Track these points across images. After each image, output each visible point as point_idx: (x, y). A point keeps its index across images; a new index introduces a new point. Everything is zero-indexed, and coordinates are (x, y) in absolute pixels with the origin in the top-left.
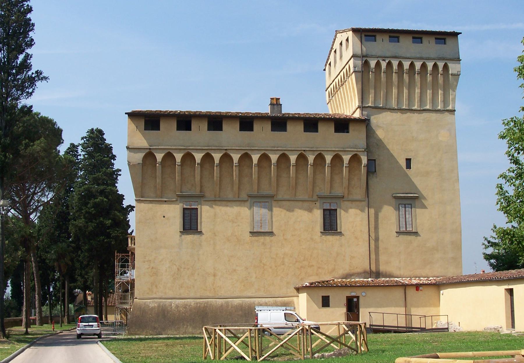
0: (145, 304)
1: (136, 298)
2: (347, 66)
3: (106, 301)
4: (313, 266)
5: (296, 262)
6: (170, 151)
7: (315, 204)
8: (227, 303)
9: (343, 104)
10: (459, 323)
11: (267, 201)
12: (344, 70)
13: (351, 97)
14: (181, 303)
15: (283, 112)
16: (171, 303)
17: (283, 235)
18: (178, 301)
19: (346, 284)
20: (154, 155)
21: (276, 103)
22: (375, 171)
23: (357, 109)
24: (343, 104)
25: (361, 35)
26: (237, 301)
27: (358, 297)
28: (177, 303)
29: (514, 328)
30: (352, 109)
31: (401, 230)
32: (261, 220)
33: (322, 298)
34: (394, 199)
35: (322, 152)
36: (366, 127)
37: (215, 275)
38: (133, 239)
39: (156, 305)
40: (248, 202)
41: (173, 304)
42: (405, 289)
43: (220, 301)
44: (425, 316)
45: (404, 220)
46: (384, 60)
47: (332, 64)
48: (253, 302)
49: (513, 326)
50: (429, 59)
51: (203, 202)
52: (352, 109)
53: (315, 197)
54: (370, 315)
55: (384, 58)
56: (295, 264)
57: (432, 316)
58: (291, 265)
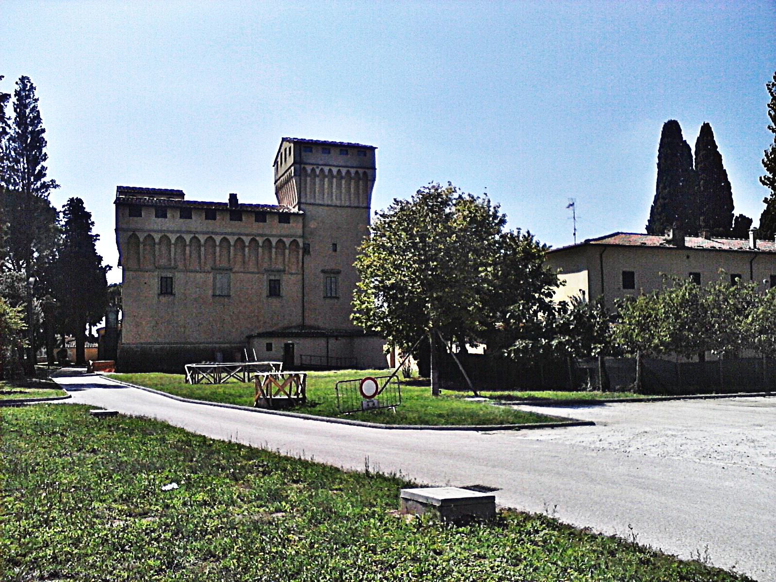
20: (184, 238)
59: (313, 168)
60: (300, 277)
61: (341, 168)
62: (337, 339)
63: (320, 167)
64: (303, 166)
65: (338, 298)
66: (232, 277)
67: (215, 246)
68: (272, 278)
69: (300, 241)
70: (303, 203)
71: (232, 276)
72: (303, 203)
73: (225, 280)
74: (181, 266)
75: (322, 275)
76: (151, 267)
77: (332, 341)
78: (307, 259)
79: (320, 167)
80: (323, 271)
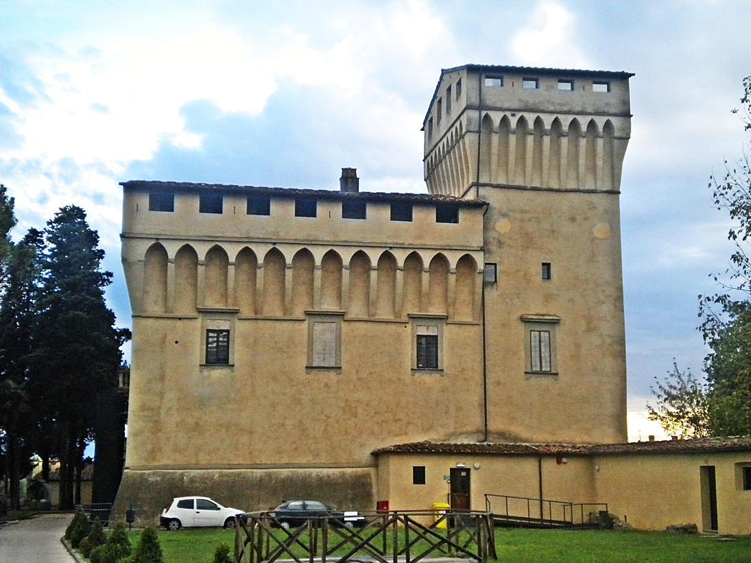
0: (142, 477)
1: (127, 468)
2: (458, 124)
3: (79, 473)
4: (400, 420)
5: (376, 413)
6: (250, 247)
7: (406, 327)
8: (269, 475)
9: (449, 181)
10: (626, 516)
11: (332, 321)
12: (453, 130)
13: (462, 170)
14: (198, 476)
15: (361, 190)
16: (182, 475)
17: (357, 372)
18: (194, 473)
19: (450, 449)
20: (163, 247)
21: (349, 177)
22: (496, 281)
23: (470, 188)
24: (449, 181)
25: (480, 76)
26: (285, 472)
27: (468, 471)
28: (192, 475)
29: (717, 529)
30: (468, 183)
31: (534, 369)
32: (324, 350)
33: (316, 212)
34: (523, 324)
35: (417, 251)
36: (484, 215)
37: (251, 433)
38: (126, 376)
39: (158, 479)
40: (305, 322)
41: (185, 478)
42: (540, 462)
43: (259, 472)
44: (571, 505)
45: (538, 354)
46: (513, 115)
47: (435, 121)
48: (309, 475)
49: (714, 525)
50: (582, 113)
51: (237, 320)
52: (468, 183)
53: (405, 319)
54: (487, 499)
55: (514, 111)
56: (374, 417)
57: (582, 504)
58: (367, 418)
59: (505, 116)
60: (479, 329)
61: (559, 116)
62: (559, 462)
63: (519, 115)
64: (484, 113)
65: (556, 374)
66: (343, 331)
67: (312, 268)
68: (423, 331)
69: (479, 259)
70: (485, 185)
71: (344, 326)
72: (485, 185)
73: (330, 337)
74: (246, 311)
75: (521, 327)
76: (188, 311)
77: (549, 466)
78: (491, 294)
79: (519, 115)
80: (524, 320)
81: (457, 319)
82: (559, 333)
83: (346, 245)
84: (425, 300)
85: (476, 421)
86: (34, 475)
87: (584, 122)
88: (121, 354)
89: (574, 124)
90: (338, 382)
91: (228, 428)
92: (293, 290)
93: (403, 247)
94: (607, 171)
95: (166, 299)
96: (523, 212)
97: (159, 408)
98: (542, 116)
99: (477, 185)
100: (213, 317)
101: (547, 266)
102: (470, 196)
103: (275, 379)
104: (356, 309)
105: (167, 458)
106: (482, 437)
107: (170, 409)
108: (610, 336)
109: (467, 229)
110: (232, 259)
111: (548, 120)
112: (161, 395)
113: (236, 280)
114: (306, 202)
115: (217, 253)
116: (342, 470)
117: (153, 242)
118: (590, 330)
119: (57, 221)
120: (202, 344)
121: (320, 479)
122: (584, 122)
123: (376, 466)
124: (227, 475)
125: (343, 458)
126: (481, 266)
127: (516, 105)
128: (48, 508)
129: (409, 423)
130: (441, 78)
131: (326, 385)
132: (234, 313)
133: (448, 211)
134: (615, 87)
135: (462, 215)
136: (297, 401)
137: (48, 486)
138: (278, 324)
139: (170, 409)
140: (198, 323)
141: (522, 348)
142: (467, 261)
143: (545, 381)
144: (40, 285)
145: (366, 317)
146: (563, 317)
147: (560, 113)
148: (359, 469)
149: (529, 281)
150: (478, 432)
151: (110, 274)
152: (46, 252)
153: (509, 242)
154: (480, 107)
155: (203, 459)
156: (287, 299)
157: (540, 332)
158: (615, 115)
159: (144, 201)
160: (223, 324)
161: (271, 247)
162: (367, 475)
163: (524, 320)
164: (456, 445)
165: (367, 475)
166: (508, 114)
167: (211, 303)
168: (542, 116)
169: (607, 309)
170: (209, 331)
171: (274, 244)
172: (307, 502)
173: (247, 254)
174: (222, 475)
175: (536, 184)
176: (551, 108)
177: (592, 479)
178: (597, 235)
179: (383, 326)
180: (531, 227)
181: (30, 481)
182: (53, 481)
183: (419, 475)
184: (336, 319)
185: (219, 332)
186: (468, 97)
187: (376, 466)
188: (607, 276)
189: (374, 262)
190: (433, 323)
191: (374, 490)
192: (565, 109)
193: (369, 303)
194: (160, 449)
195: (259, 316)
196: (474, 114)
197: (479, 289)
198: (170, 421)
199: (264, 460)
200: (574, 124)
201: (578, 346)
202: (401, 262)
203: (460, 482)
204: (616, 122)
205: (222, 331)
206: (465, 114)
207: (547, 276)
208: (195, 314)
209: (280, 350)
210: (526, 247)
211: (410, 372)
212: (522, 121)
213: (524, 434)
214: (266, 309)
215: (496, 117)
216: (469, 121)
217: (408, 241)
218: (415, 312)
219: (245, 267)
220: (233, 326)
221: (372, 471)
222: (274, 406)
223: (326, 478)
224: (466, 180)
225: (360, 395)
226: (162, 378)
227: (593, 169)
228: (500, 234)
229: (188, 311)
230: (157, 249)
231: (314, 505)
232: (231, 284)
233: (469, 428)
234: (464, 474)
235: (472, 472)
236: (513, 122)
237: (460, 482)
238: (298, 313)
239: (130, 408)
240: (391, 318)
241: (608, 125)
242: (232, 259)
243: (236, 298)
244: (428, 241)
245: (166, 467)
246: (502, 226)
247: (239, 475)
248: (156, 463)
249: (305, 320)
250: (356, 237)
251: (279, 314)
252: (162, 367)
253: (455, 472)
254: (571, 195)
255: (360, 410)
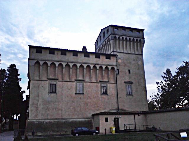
8: (67, 121)
16: (44, 122)
21: (84, 48)
26: (71, 120)
43: (64, 120)
50: (135, 37)
55: (121, 36)
57: (129, 125)
60: (115, 85)
62: (139, 115)
63: (122, 36)
64: (115, 35)
68: (103, 85)
69: (115, 68)
70: (115, 52)
72: (115, 52)
73: (81, 86)
74: (60, 79)
75: (125, 84)
76: (46, 79)
77: (136, 116)
80: (125, 82)
81: (111, 82)
82: (133, 85)
83: (85, 63)
84: (103, 78)
85: (116, 106)
86: (3, 123)
87: (135, 39)
88: (23, 96)
89: (133, 39)
90: (83, 97)
91: (56, 109)
92: (72, 74)
93: (98, 64)
94: (140, 50)
95: (39, 76)
96: (124, 58)
97: (37, 104)
98: (127, 37)
99: (113, 51)
100: (52, 80)
101: (129, 71)
102: (112, 53)
103: (68, 97)
104: (87, 79)
105: (40, 117)
106: (117, 110)
107: (40, 104)
108: (143, 86)
109: (112, 62)
110: (57, 66)
111: (128, 38)
112: (38, 100)
113: (58, 72)
114: (75, 53)
115: (53, 64)
116: (66, 120)
117: (37, 61)
118: (139, 85)
119: (9, 67)
120: (49, 88)
121: (79, 122)
122: (135, 39)
123: (93, 118)
124: (56, 121)
125: (85, 116)
126: (116, 69)
127: (121, 34)
128: (6, 130)
129: (100, 107)
130: (101, 31)
131: (80, 98)
132: (57, 79)
133: (108, 57)
134: (141, 32)
135: (111, 57)
136: (73, 102)
137: (6, 125)
138: (68, 83)
139: (40, 104)
140: (48, 82)
141: (125, 89)
142: (113, 68)
143: (131, 97)
144: (5, 81)
145: (89, 81)
146: (133, 82)
147: (131, 37)
148: (86, 119)
149: (126, 74)
150: (116, 109)
151: (21, 79)
152: (7, 74)
153: (121, 65)
154: (114, 34)
155: (49, 117)
156: (71, 76)
157: (129, 85)
158: (141, 38)
159: (35, 50)
160: (55, 83)
161: (66, 63)
162: (91, 121)
163: (125, 82)
164: (112, 112)
165: (91, 121)
166: (120, 36)
167: (51, 77)
168: (127, 37)
169: (142, 80)
170: (51, 84)
171: (68, 62)
172: (83, 128)
173: (61, 65)
174: (54, 121)
175: (126, 52)
176: (129, 35)
177: (146, 119)
178: (139, 64)
179: (94, 84)
180: (125, 61)
181: (2, 124)
182: (7, 124)
183: (107, 120)
184: (83, 82)
185: (53, 84)
186: (111, 32)
187: (93, 118)
188: (142, 73)
189: (92, 68)
190: (105, 83)
191: (93, 124)
192: (131, 36)
193: (90, 78)
194: (38, 115)
195: (64, 80)
196: (113, 36)
197: (115, 75)
198: (41, 107)
199: (65, 117)
200: (133, 39)
201: (137, 89)
202: (98, 68)
203: (116, 121)
204: (142, 40)
205: (54, 84)
206: (111, 36)
207: (129, 72)
208: (47, 80)
209: (69, 89)
210: (125, 66)
211: (100, 95)
212: (123, 38)
213: (127, 109)
214: (65, 79)
215: (117, 37)
216: (112, 37)
217: (100, 63)
218: (101, 80)
219: (60, 68)
220: (57, 83)
221: (92, 119)
222: (68, 103)
223: (84, 122)
224: (110, 51)
225: (89, 100)
226: (38, 96)
227: (137, 49)
228: (119, 63)
229: (46, 79)
230: (38, 63)
231: (84, 129)
232: (56, 72)
233: (114, 108)
234: (117, 119)
235: (119, 118)
236: (121, 38)
237: (116, 121)
238: (73, 80)
239: (30, 104)
240: (96, 81)
241: (140, 40)
242: (57, 66)
243: (57, 76)
244: (104, 63)
245: (39, 119)
246: (120, 61)
247: (59, 121)
248: (37, 119)
249: (74, 82)
250: (88, 62)
251: (68, 80)
252: (38, 93)
253: (115, 119)
254: (133, 55)
255: (89, 104)
